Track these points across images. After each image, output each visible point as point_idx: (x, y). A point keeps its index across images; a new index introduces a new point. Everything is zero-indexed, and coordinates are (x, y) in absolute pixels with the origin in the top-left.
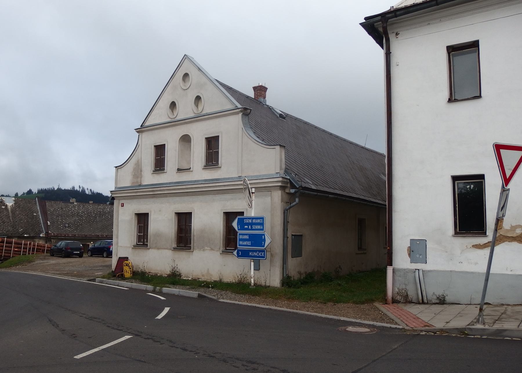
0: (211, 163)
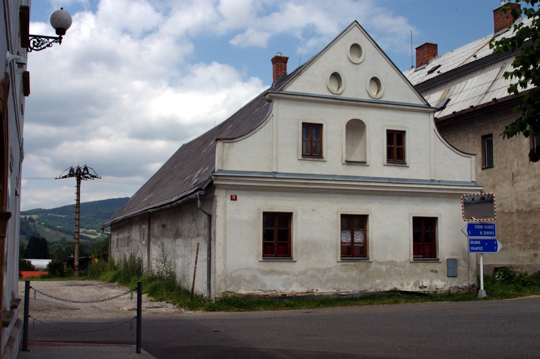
0: (394, 160)
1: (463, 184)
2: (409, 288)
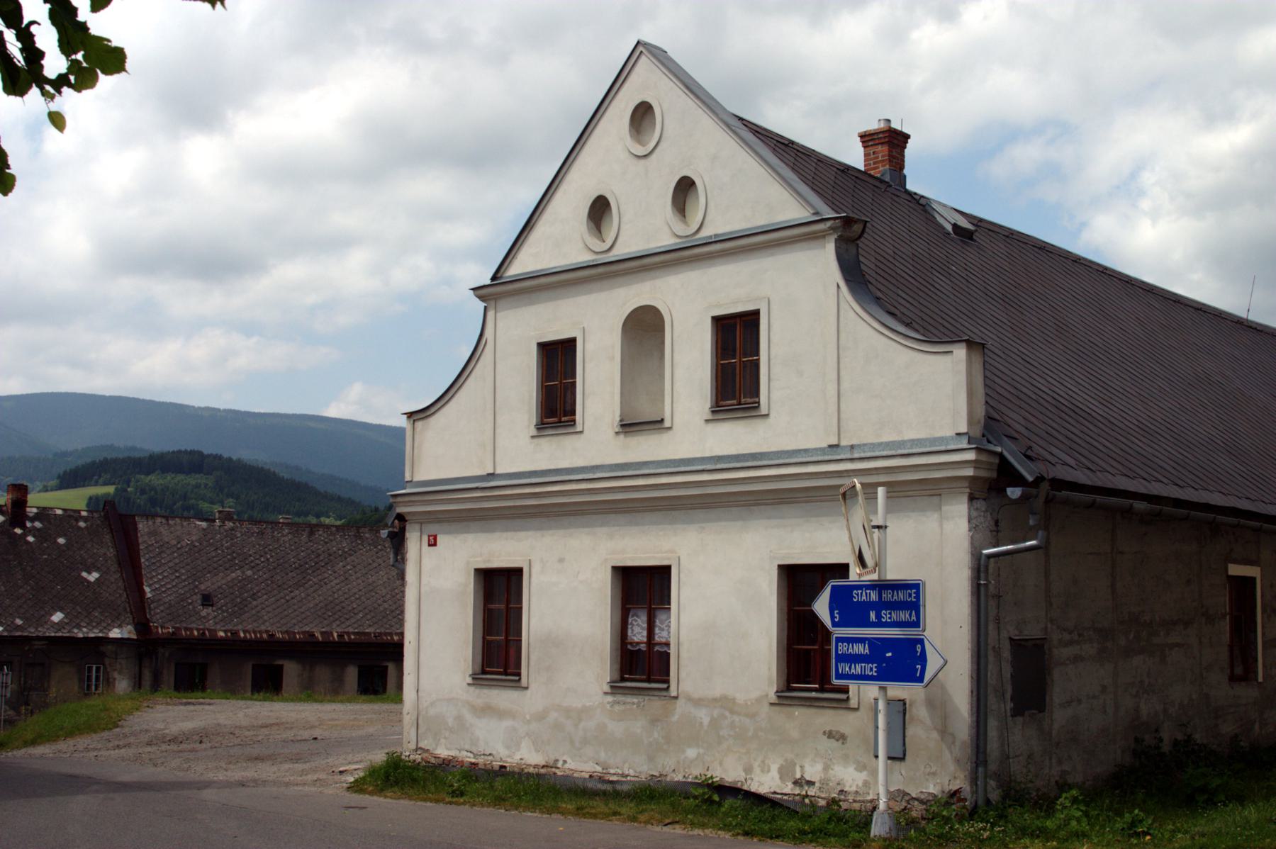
0: (735, 402)
1: (926, 446)
2: (766, 782)
